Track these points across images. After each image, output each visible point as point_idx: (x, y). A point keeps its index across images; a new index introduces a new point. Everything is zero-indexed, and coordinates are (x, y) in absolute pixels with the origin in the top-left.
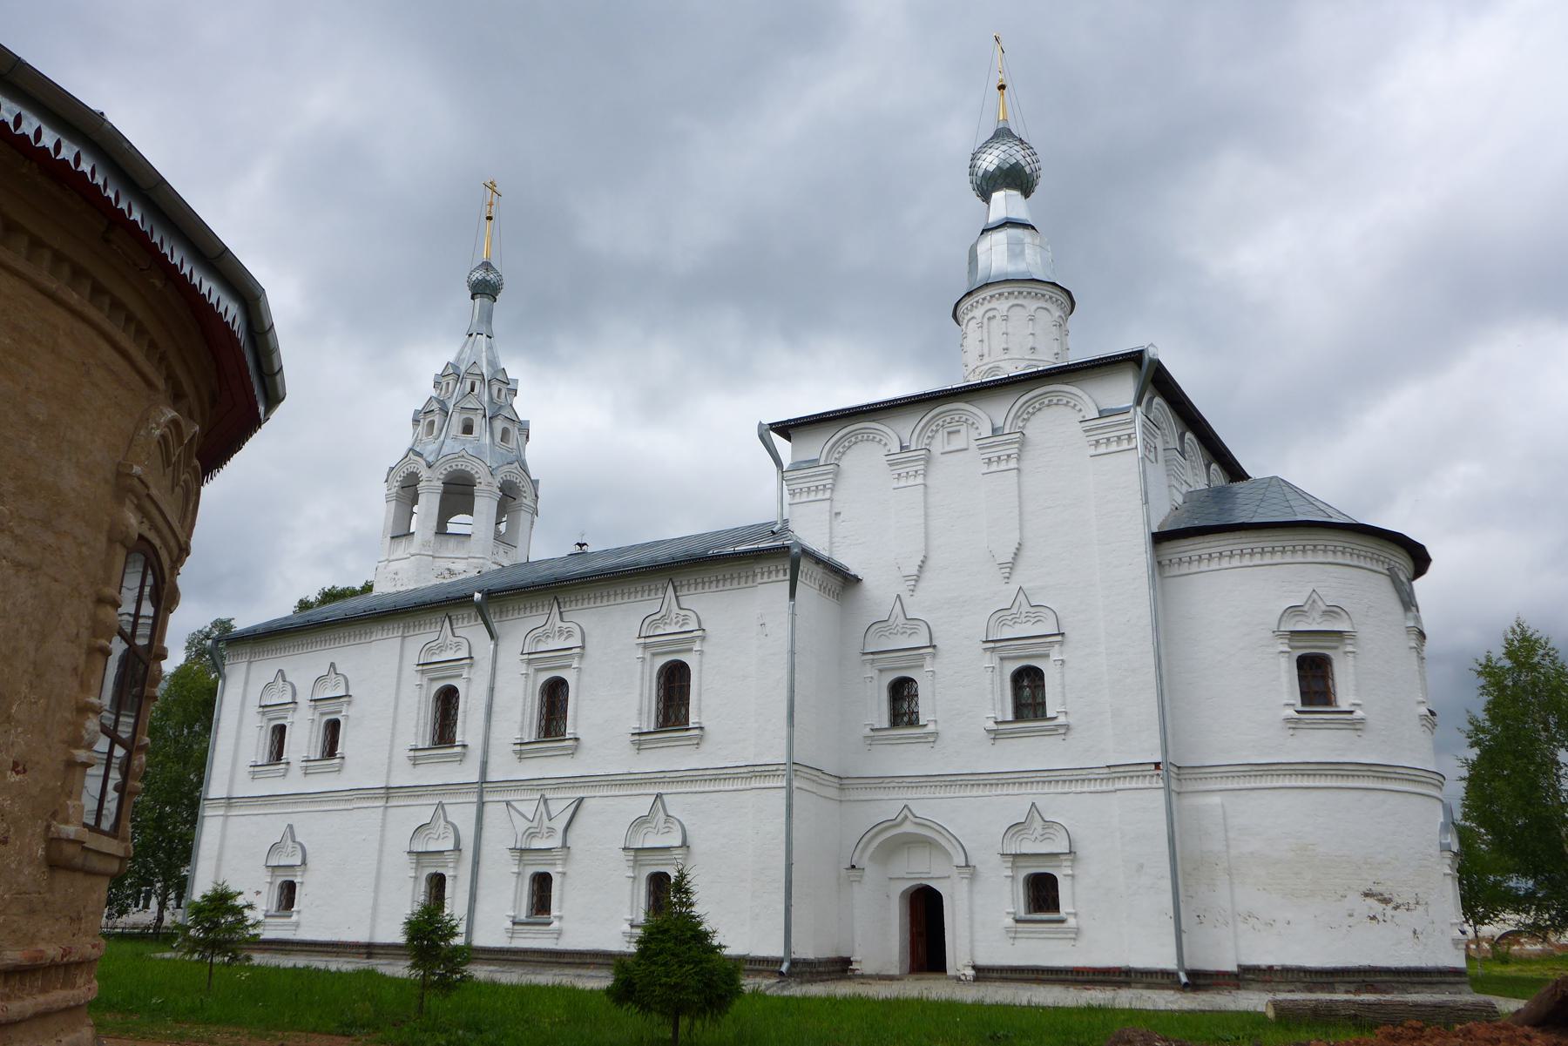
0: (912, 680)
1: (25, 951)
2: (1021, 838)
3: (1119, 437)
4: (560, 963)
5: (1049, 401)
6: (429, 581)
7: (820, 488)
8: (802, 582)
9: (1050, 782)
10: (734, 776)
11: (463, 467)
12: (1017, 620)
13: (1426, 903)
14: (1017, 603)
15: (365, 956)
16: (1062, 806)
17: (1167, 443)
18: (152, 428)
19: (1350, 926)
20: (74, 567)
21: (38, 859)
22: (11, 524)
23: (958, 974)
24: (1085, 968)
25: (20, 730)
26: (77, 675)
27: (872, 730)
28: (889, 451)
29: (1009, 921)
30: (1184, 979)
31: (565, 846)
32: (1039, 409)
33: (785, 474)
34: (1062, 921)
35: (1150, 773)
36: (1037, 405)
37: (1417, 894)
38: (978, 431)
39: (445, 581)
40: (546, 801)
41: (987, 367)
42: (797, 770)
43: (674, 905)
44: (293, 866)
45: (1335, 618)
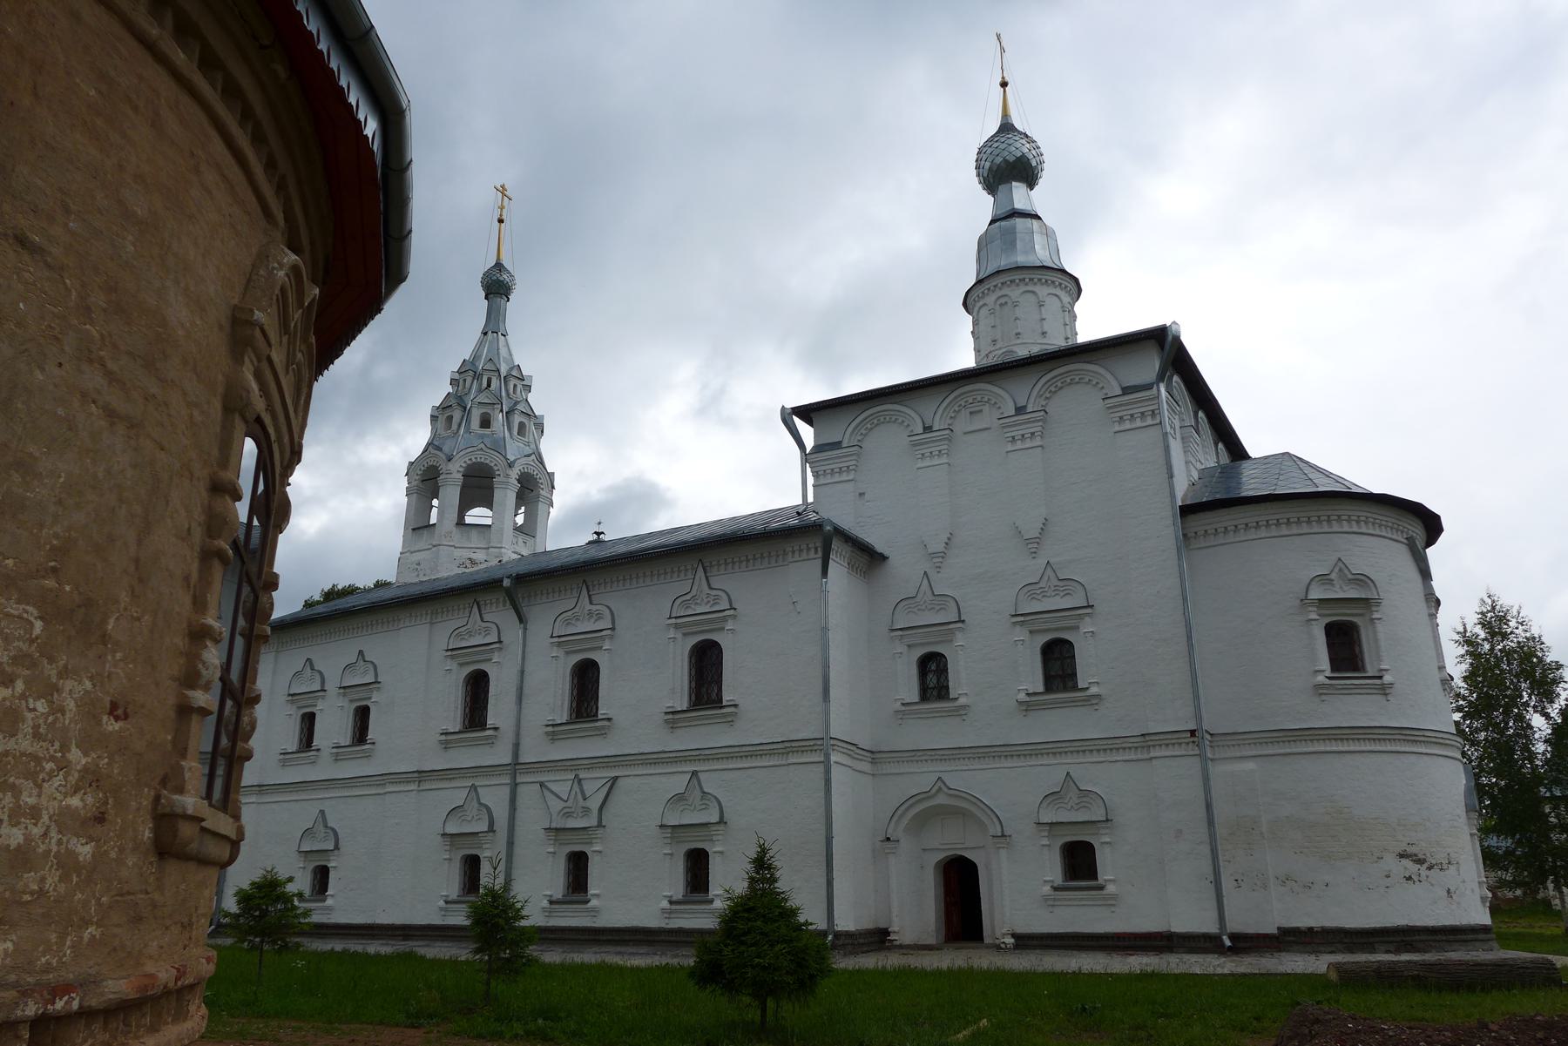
1: (132, 979)
2: (1057, 807)
3: (1142, 413)
4: (599, 941)
5: (1071, 380)
6: (452, 570)
7: (828, 471)
11: (482, 460)
12: (1045, 594)
13: (1457, 863)
15: (401, 938)
16: (1098, 776)
17: (1183, 420)
18: (274, 268)
20: (184, 434)
21: (145, 843)
22: (102, 353)
23: (997, 942)
24: (1125, 933)
25: (119, 656)
26: (189, 586)
27: (903, 704)
28: (912, 431)
29: (1047, 889)
30: (1228, 943)
31: (600, 825)
32: (1061, 388)
33: (808, 457)
34: (1101, 888)
35: (1186, 741)
36: (1059, 384)
39: (467, 571)
40: (580, 781)
43: (757, 881)
44: (327, 851)
45: (1362, 586)
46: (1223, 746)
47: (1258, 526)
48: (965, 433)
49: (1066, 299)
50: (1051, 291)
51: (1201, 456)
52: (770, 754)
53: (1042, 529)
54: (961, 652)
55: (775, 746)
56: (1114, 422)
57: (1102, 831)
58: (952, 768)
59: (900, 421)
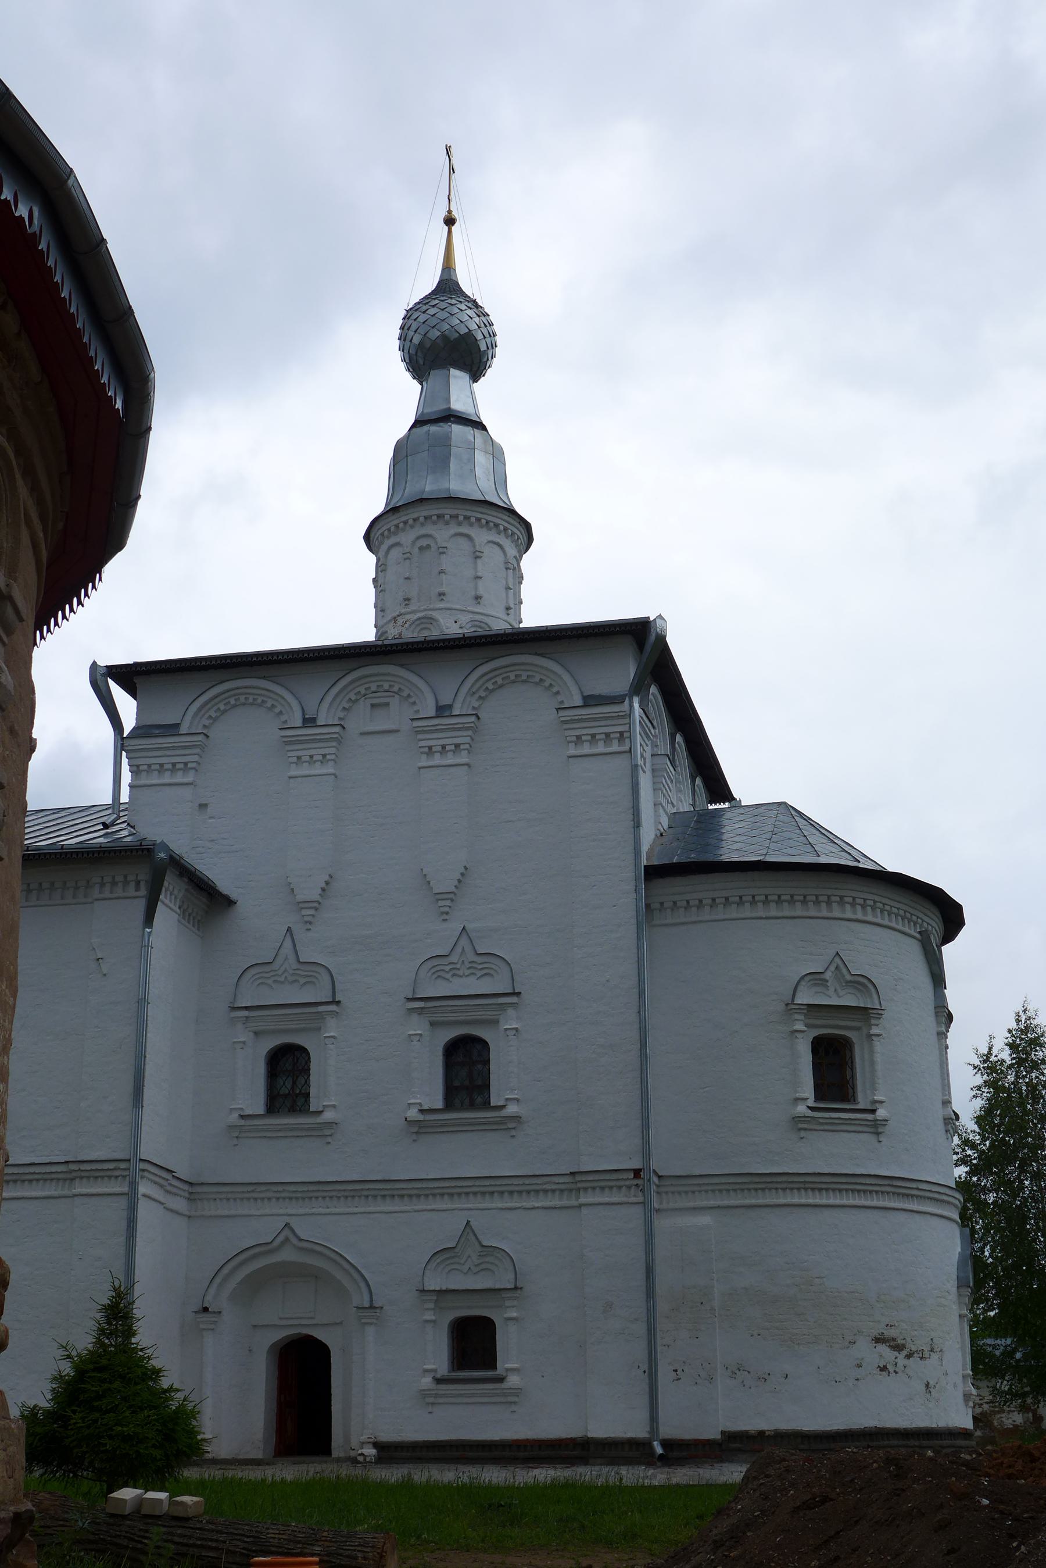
0: (303, 1050)
3: (607, 735)
7: (178, 766)
8: (163, 903)
9: (492, 1193)
10: (45, 1176)
13: (941, 1351)
14: (459, 949)
17: (657, 746)
19: (857, 1380)
23: (353, 1454)
27: (242, 1117)
28: (285, 722)
29: (427, 1381)
30: (659, 1450)
32: (501, 686)
33: (126, 742)
35: (628, 1183)
36: (499, 681)
37: (932, 1339)
38: (415, 708)
41: (416, 617)
42: (143, 1170)
46: (673, 1193)
47: (741, 902)
48: (363, 734)
49: (512, 551)
50: (491, 538)
51: (673, 796)
52: (45, 1180)
53: (459, 881)
54: (332, 1046)
55: (54, 1169)
56: (569, 742)
57: (508, 1303)
58: (307, 1210)
59: (269, 705)
